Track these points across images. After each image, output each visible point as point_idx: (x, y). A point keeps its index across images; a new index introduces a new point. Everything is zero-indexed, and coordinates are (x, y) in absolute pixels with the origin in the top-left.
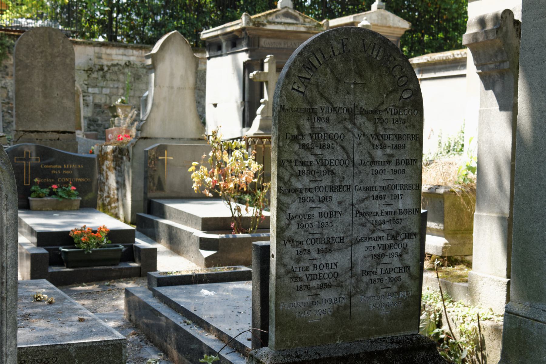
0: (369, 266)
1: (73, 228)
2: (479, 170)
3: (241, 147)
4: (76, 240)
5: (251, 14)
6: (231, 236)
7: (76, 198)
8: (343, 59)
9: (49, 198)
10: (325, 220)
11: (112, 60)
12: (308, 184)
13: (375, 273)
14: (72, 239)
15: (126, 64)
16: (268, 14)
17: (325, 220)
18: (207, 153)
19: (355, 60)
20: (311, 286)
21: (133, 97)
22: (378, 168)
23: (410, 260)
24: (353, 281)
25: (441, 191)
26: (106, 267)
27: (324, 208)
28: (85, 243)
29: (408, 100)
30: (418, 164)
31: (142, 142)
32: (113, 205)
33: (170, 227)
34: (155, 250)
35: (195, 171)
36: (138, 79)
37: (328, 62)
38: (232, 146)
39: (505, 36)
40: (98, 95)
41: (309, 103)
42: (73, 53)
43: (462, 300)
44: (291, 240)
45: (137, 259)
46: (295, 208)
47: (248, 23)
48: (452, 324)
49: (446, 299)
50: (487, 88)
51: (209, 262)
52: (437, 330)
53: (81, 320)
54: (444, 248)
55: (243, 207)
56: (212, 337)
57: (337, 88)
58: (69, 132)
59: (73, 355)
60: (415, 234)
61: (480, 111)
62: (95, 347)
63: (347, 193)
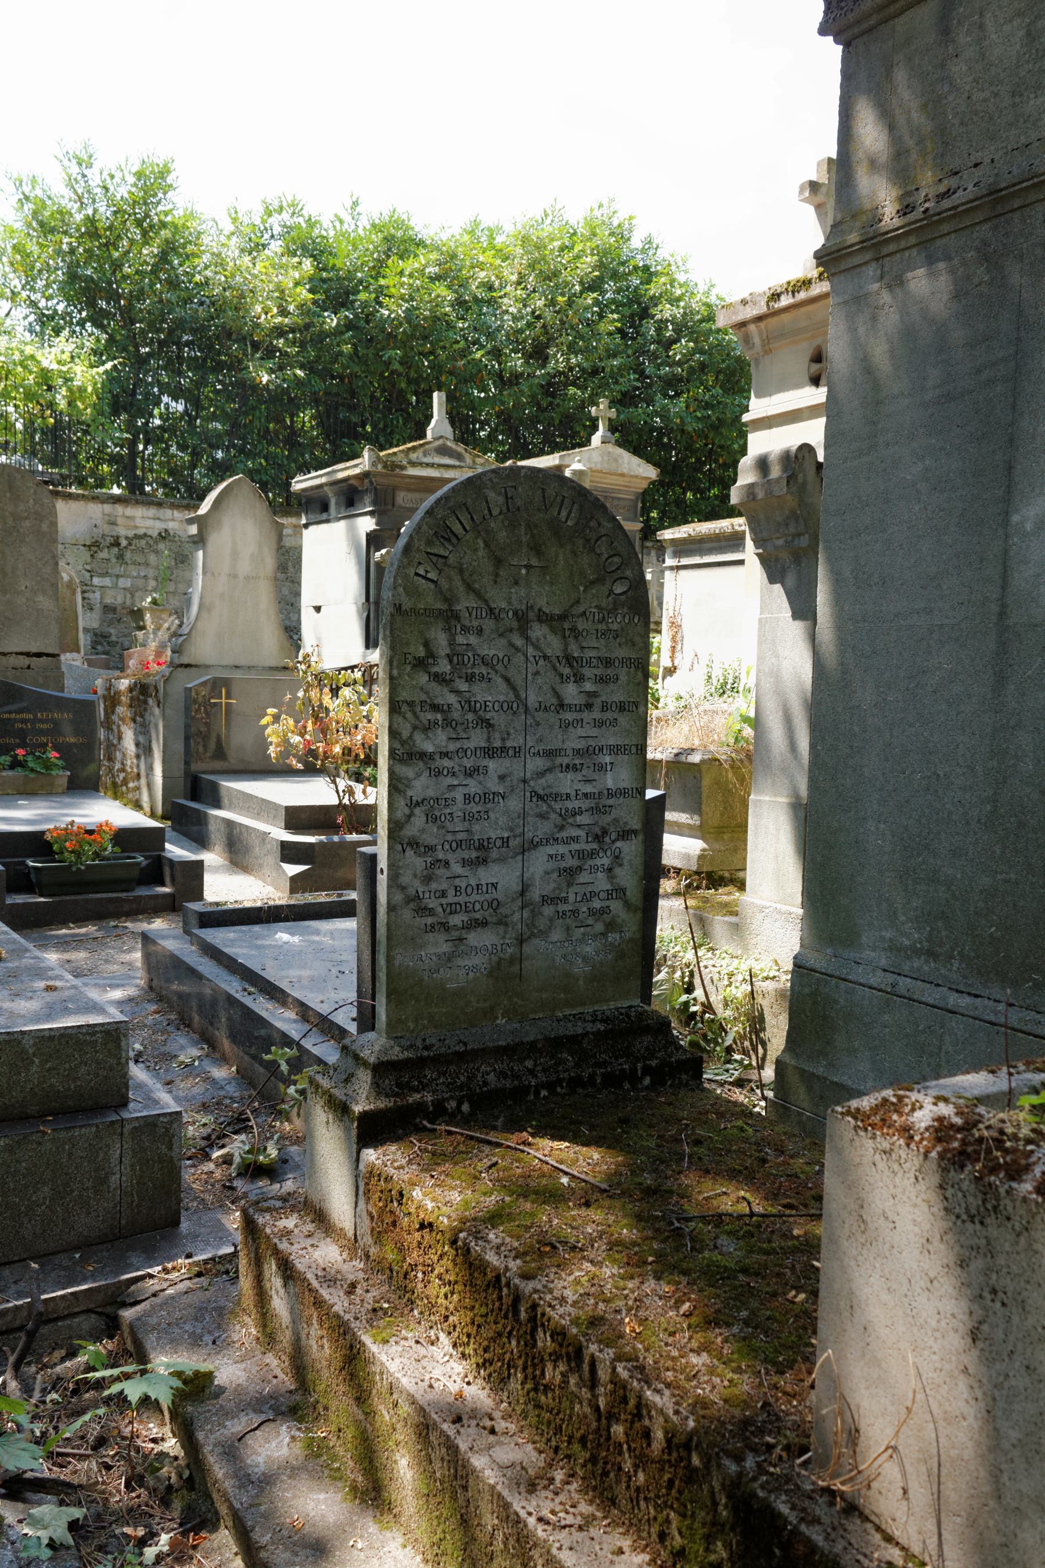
0: (554, 890)
1: (51, 826)
2: (756, 723)
3: (355, 682)
4: (55, 847)
5: (382, 449)
6: (336, 838)
7: (61, 773)
8: (506, 523)
9: (10, 773)
10: (474, 808)
11: (136, 527)
12: (444, 744)
13: (565, 900)
14: (49, 845)
15: (160, 534)
16: (409, 449)
17: (474, 808)
18: (294, 693)
19: (528, 525)
20: (451, 924)
21: (174, 593)
22: (569, 716)
23: (628, 878)
24: (525, 915)
25: (695, 758)
26: (110, 895)
27: (473, 787)
28: (72, 852)
29: (623, 597)
30: (641, 709)
31: (181, 673)
32: (131, 785)
33: (230, 824)
34: (200, 864)
35: (273, 723)
36: (182, 562)
37: (480, 528)
38: (338, 680)
39: (803, 488)
40: (110, 589)
41: (446, 600)
42: (53, 512)
43: (724, 943)
44: (414, 844)
45: (168, 880)
46: (421, 786)
47: (374, 464)
48: (710, 988)
49: (701, 945)
50: (772, 580)
51: (297, 884)
52: (684, 998)
53: (49, 989)
54: (701, 857)
55: (358, 788)
56: (291, 1014)
57: (497, 575)
58: (48, 655)
59: (31, 1051)
60: (635, 832)
61: (760, 620)
62: (70, 1036)
63: (515, 760)
